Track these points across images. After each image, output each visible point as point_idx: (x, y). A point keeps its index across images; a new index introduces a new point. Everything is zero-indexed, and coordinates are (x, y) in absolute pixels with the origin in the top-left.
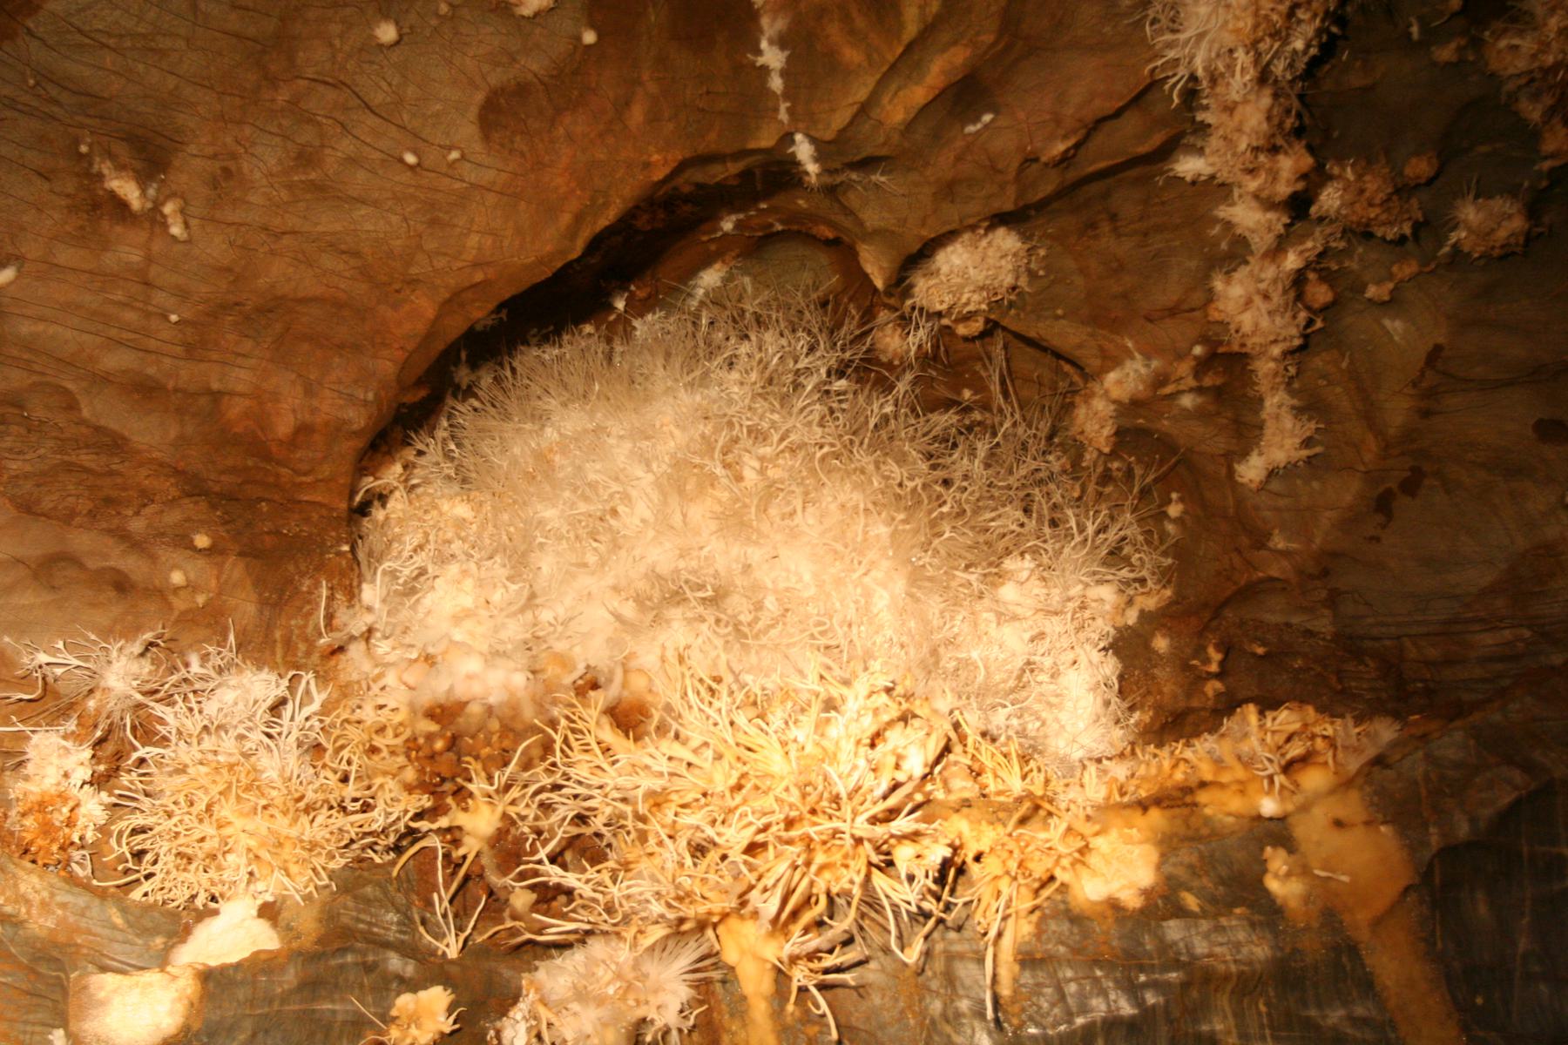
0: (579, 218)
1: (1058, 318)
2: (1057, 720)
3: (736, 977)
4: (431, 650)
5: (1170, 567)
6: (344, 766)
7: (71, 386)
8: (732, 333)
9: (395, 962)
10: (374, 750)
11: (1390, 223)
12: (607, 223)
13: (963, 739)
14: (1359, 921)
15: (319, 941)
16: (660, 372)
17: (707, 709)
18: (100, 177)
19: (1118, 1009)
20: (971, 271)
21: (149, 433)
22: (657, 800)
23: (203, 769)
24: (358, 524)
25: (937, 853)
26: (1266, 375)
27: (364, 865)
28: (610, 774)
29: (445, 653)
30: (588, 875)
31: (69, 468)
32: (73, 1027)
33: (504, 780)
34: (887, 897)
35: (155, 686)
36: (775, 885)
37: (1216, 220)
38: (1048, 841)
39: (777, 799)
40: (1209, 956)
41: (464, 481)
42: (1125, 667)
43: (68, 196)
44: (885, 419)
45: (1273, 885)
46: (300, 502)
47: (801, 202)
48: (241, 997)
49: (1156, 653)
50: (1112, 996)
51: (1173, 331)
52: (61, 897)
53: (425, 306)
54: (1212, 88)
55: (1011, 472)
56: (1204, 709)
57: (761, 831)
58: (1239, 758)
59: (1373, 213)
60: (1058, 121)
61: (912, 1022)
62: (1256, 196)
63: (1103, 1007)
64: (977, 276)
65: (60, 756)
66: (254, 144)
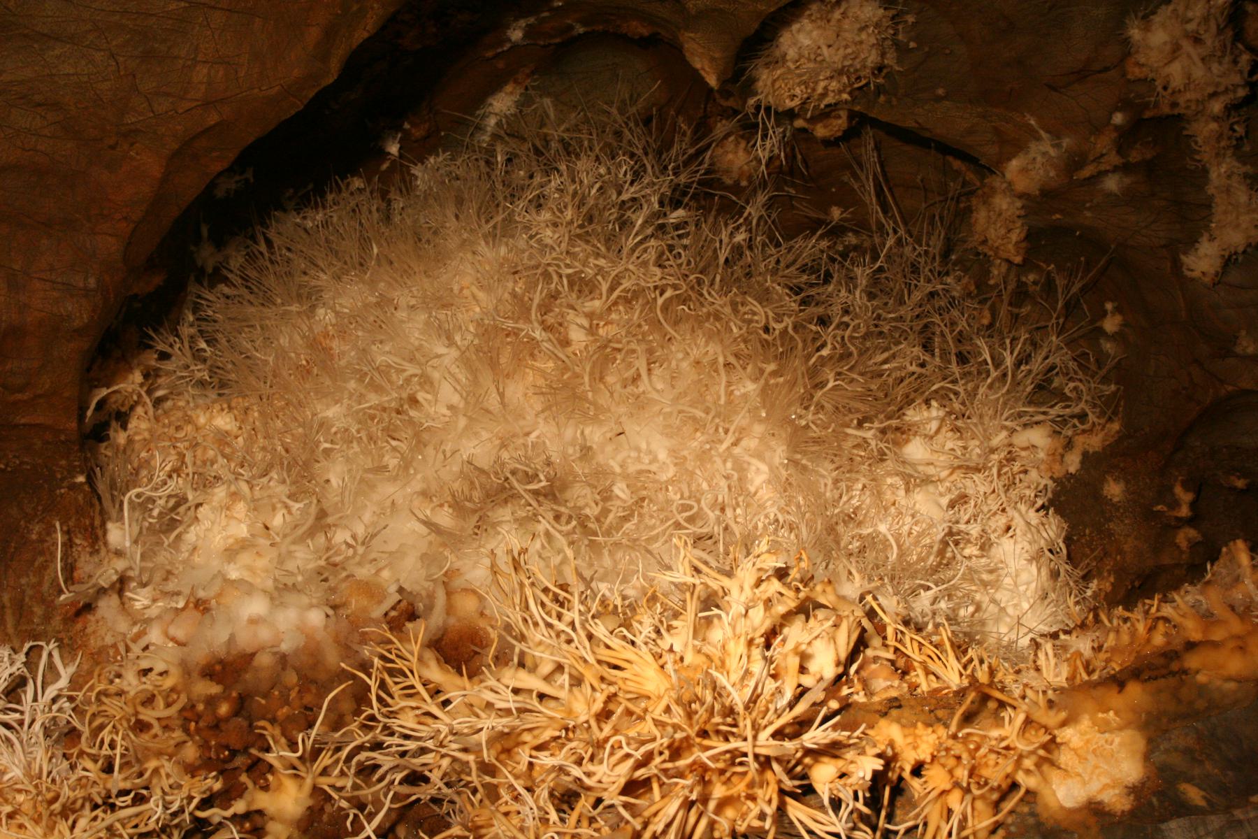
1: (939, 99)
2: (993, 601)
4: (201, 594)
5: (1114, 394)
6: (106, 751)
10: (141, 727)
12: (366, 35)
13: (881, 629)
16: (452, 223)
17: (555, 622)
20: (825, 51)
22: (506, 743)
25: (865, 767)
28: (447, 719)
29: (220, 595)
33: (309, 744)
38: (1003, 739)
39: (658, 723)
41: (223, 385)
44: (737, 251)
46: (16, 426)
53: (150, 163)
55: (902, 302)
57: (640, 765)
58: (1232, 608)
64: (833, 56)
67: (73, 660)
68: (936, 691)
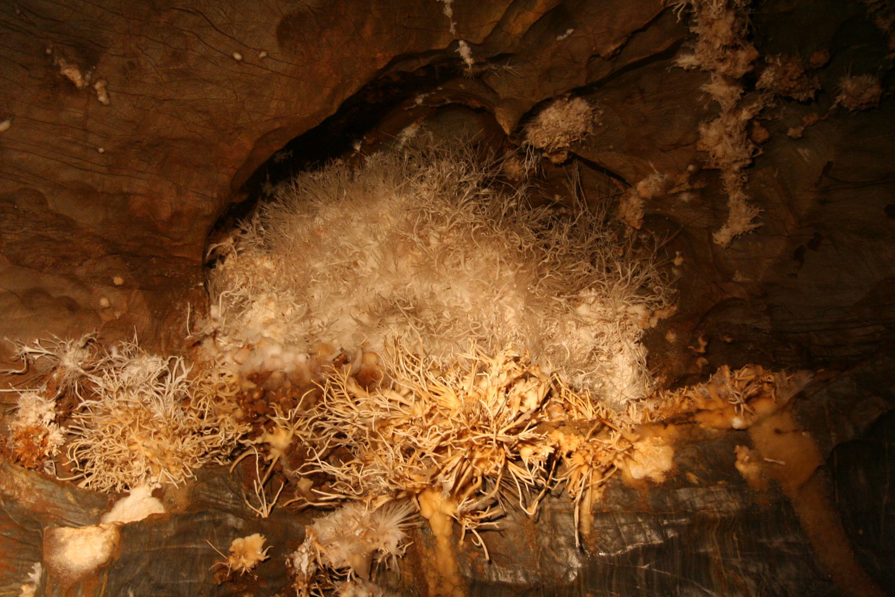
1: (610, 150)
2: (611, 382)
3: (430, 525)
4: (251, 342)
5: (675, 294)
6: (201, 408)
7: (42, 190)
9: (231, 520)
10: (218, 399)
11: (802, 91)
13: (559, 390)
15: (188, 509)
16: (381, 184)
17: (411, 371)
18: (58, 68)
19: (652, 541)
21: (88, 217)
22: (383, 423)
23: (120, 412)
24: (209, 273)
27: (213, 466)
28: (356, 410)
29: (259, 343)
30: (343, 468)
32: (46, 559)
33: (293, 415)
34: (518, 478)
35: (91, 365)
36: (452, 471)
37: (702, 93)
39: (453, 421)
40: (705, 508)
41: (269, 248)
43: (40, 79)
44: (511, 210)
45: (741, 467)
47: (461, 86)
48: (143, 541)
49: (668, 342)
50: (648, 533)
53: (246, 142)
54: (700, 12)
55: (583, 242)
56: (696, 374)
57: (443, 439)
58: (720, 396)
61: (532, 550)
62: (724, 76)
63: (643, 539)
64: (564, 126)
65: (37, 406)
67: (190, 365)
68: (580, 420)
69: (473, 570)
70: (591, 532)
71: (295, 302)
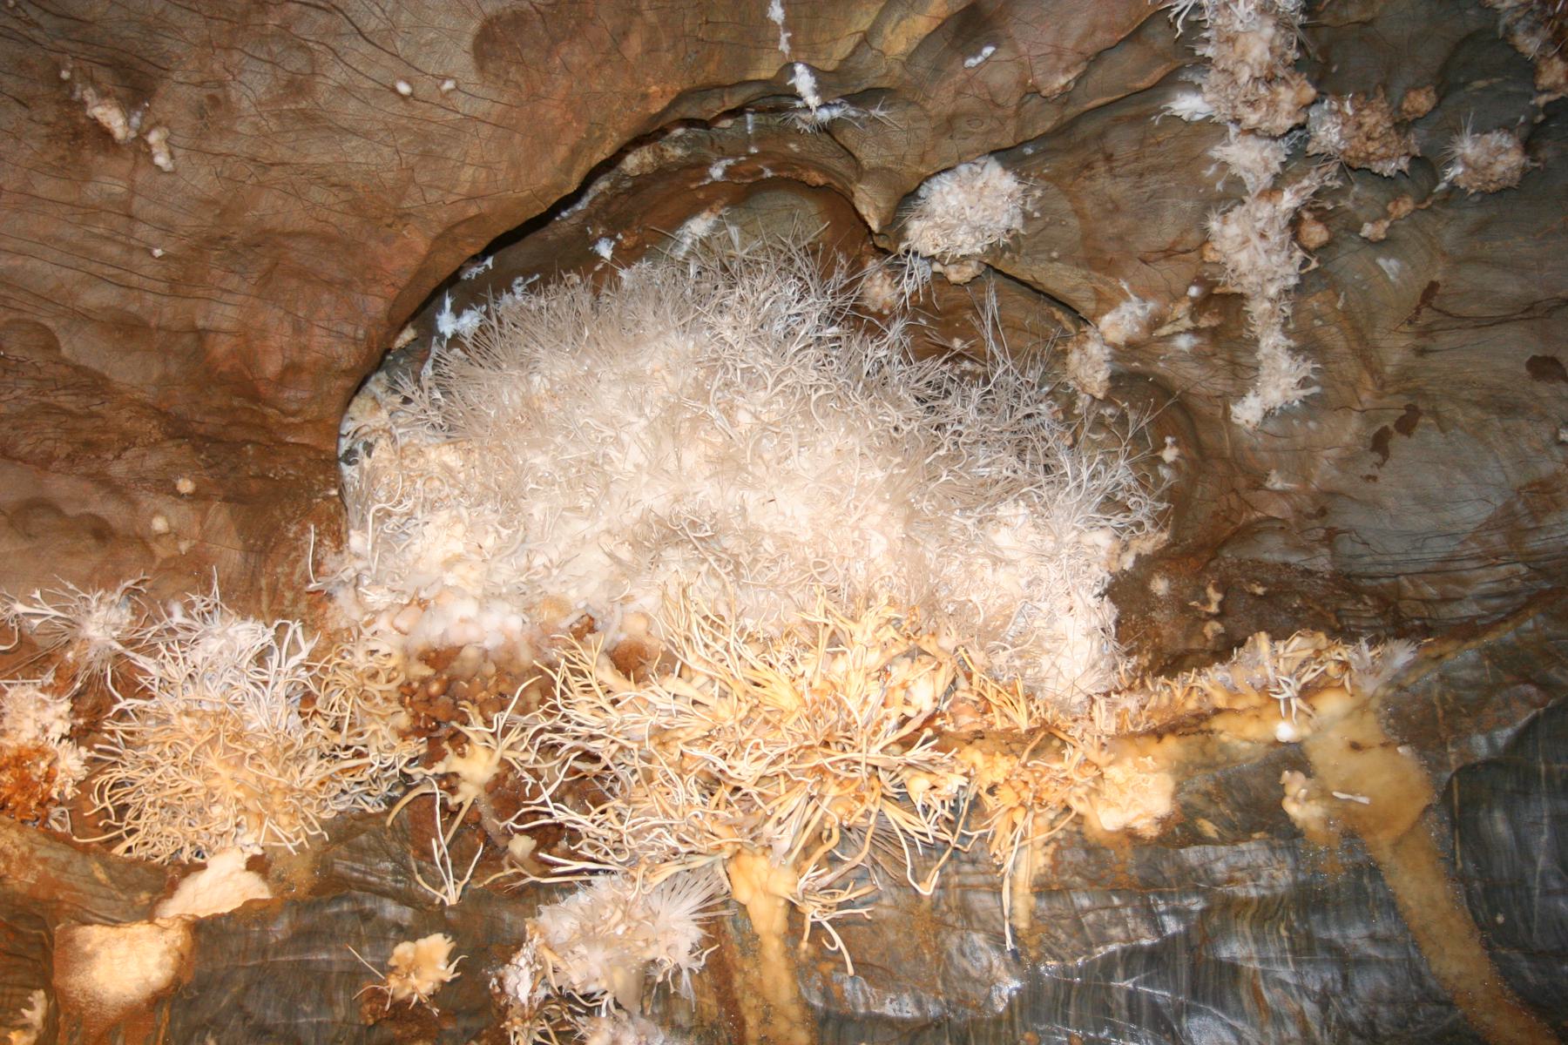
0: (575, 152)
1: (1052, 260)
3: (748, 916)
4: (423, 595)
5: (1166, 511)
7: (50, 324)
8: (720, 283)
9: (391, 910)
11: (1390, 158)
14: (1382, 844)
15: (314, 891)
16: (650, 318)
18: (82, 104)
21: (132, 372)
23: (187, 720)
26: (1261, 316)
28: (605, 713)
29: (438, 596)
30: (591, 816)
31: (48, 410)
32: (57, 981)
34: (903, 830)
37: (1212, 161)
42: (1122, 613)
43: (48, 124)
45: (1292, 809)
46: (287, 444)
47: (792, 146)
51: (1165, 272)
52: (42, 852)
53: (418, 241)
56: (1203, 651)
57: (773, 763)
59: (1372, 147)
60: (1059, 54)
66: (242, 71)
67: (313, 637)
68: (1008, 730)
69: (826, 994)
70: (1032, 925)
71: (502, 524)
